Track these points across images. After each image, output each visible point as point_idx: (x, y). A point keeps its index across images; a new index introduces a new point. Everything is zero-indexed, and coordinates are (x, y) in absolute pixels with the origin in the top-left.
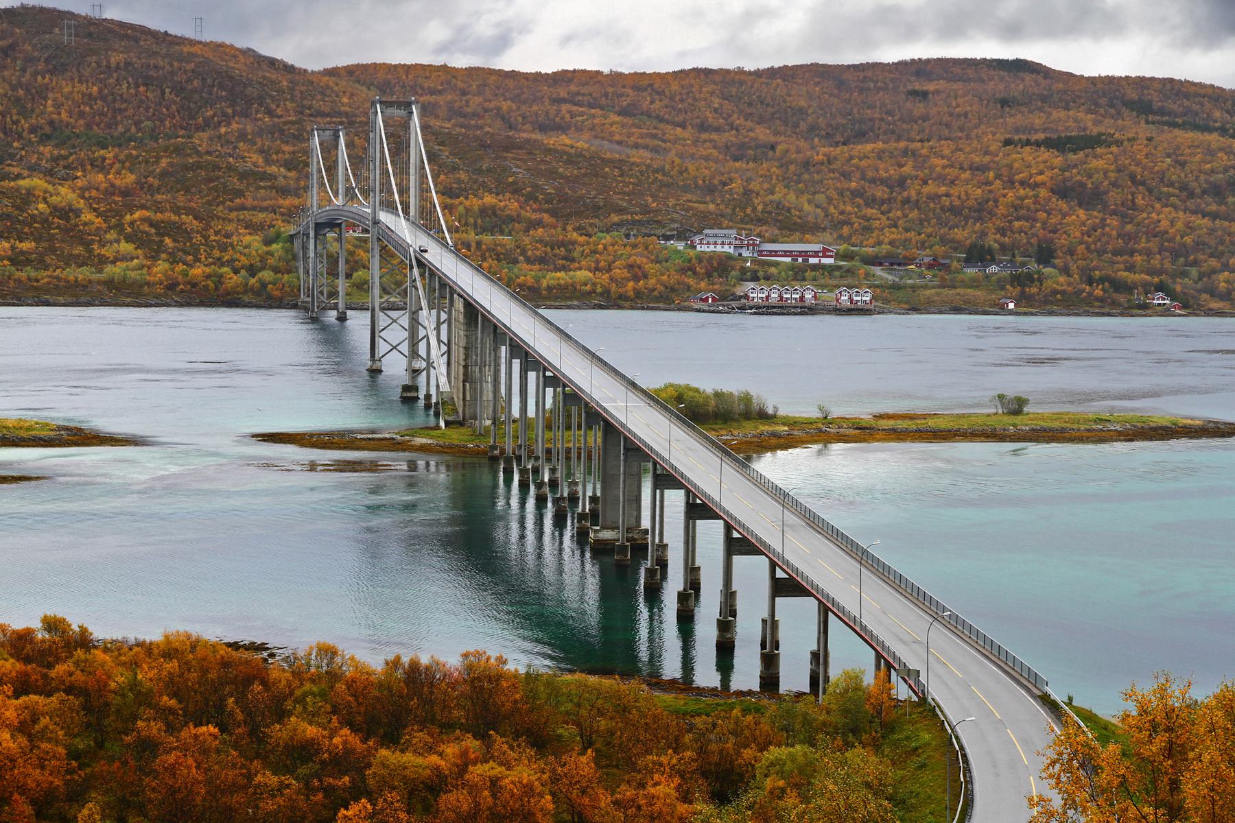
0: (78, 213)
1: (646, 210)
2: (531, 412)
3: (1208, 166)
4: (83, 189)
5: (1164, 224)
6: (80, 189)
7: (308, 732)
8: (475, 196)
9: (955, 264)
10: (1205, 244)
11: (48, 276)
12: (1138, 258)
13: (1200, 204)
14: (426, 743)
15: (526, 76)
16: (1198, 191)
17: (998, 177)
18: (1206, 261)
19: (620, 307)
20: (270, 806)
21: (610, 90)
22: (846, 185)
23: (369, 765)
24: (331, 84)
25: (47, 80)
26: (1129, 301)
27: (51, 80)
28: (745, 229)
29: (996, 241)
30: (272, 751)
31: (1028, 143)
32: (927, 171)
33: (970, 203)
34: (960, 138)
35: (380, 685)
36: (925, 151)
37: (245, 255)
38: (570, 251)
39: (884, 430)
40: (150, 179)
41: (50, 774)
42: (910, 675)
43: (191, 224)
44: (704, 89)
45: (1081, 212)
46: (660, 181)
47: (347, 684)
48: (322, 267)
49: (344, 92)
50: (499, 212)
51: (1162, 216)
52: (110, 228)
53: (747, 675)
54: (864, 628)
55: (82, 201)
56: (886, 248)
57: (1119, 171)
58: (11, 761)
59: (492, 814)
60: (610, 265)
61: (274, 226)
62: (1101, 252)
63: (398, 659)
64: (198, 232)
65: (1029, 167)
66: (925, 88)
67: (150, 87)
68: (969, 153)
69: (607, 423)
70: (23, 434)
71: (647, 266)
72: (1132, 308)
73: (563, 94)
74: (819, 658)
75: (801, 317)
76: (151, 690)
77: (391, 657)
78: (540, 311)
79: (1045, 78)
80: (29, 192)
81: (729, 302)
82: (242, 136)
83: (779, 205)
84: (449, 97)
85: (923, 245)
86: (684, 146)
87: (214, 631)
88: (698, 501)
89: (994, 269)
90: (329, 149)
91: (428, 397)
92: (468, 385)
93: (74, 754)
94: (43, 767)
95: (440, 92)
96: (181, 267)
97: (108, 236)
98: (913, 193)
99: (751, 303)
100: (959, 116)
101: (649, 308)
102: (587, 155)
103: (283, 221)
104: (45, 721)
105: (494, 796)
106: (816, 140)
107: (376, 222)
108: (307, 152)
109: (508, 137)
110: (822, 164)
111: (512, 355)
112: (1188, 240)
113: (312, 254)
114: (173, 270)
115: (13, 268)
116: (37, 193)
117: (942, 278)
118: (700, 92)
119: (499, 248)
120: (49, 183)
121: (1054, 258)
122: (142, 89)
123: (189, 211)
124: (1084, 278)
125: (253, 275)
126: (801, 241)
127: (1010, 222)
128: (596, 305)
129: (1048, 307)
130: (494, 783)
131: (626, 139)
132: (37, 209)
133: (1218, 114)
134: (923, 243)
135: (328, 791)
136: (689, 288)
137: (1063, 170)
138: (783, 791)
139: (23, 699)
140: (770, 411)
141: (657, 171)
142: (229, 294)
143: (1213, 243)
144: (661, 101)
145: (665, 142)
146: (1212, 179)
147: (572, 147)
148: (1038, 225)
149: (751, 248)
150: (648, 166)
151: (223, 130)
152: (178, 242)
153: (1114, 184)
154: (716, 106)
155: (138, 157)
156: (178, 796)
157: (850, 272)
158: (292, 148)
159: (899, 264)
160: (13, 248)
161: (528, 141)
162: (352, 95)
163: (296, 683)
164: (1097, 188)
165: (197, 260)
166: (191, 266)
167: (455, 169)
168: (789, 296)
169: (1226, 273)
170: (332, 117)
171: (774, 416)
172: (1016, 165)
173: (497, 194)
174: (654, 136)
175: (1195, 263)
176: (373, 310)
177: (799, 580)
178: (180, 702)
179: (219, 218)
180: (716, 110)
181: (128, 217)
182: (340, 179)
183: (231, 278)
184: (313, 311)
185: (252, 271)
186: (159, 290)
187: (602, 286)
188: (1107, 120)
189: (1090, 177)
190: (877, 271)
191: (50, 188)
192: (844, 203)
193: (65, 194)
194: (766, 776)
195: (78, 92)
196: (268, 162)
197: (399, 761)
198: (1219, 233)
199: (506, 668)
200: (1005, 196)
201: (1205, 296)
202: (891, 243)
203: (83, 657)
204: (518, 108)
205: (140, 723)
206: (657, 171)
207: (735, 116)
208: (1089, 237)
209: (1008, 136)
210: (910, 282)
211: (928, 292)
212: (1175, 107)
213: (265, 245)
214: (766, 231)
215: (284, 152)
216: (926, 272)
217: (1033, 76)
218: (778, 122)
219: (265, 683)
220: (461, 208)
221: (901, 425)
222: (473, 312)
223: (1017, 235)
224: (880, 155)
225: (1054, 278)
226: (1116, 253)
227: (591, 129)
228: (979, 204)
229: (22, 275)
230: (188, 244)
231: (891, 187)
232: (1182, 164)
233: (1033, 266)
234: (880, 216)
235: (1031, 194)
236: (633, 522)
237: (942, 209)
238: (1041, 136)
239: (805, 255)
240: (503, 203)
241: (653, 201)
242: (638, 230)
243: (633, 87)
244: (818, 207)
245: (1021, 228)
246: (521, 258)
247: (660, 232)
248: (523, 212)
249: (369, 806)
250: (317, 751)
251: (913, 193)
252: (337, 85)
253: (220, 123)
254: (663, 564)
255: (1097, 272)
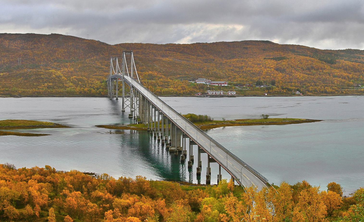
0: (61, 77)
1: (185, 74)
2: (157, 120)
3: (307, 64)
4: (63, 72)
5: (298, 76)
6: (62, 72)
7: (100, 194)
8: (147, 72)
9: (254, 85)
10: (307, 80)
11: (55, 91)
12: (293, 84)
13: (305, 72)
14: (127, 197)
15: (159, 45)
16: (305, 69)
17: (263, 66)
18: (307, 84)
19: (180, 96)
20: (90, 210)
21: (177, 48)
22: (230, 68)
23: (113, 202)
24: (116, 48)
25: (56, 49)
26: (291, 93)
27: (57, 49)
28: (207, 78)
29: (263, 80)
30: (92, 198)
31: (269, 59)
32: (247, 65)
33: (257, 72)
34: (255, 58)
35: (117, 184)
36: (247, 61)
37: (96, 86)
38: (168, 83)
39: (237, 123)
40: (77, 69)
41: (44, 201)
42: (238, 180)
43: (85, 79)
44: (199, 47)
45: (281, 74)
46: (188, 68)
47: (110, 183)
48: (113, 88)
49: (119, 49)
50: (152, 75)
51: (298, 74)
52: (68, 80)
53: (203, 181)
54: (228, 169)
55: (62, 74)
56: (239, 82)
57: (288, 65)
58: (36, 197)
59: (140, 214)
60: (177, 87)
61: (103, 79)
62: (285, 83)
63: (122, 177)
64: (86, 81)
65: (269, 64)
66: (247, 47)
67: (77, 50)
68: (257, 61)
69: (173, 123)
70: (47, 125)
71: (186, 87)
72: (292, 95)
73: (167, 49)
74: (220, 176)
75: (220, 98)
76: (67, 183)
77: (120, 177)
78: (159, 97)
79: (273, 45)
80: (52, 73)
81: (204, 95)
82: (96, 60)
83: (215, 73)
84: (142, 50)
85: (247, 81)
86: (194, 60)
87: (82, 170)
88: (201, 148)
89: (262, 86)
90: (114, 62)
91: (135, 117)
92: (143, 114)
93: (50, 196)
94: (43, 199)
95: (140, 49)
96: (82, 88)
97: (67, 82)
98: (244, 70)
99: (209, 95)
100: (254, 53)
101: (186, 96)
102: (172, 62)
103: (105, 78)
104: (44, 189)
105: (141, 210)
106: (223, 58)
107: (124, 78)
108: (110, 63)
109: (154, 58)
110: (224, 64)
111: (152, 108)
112: (303, 79)
113: (110, 85)
114: (81, 89)
115: (47, 89)
116: (53, 73)
117: (251, 88)
118: (198, 48)
119: (152, 83)
120: (56, 71)
121: (275, 84)
122: (76, 50)
123: (84, 76)
124: (282, 88)
125: (98, 90)
126: (220, 81)
127: (266, 76)
128: (174, 96)
129: (274, 95)
130: (141, 208)
131: (181, 58)
132: (53, 76)
133: (309, 53)
134: (247, 81)
135: (104, 207)
136: (195, 91)
137: (276, 65)
138: (207, 208)
139: (40, 184)
140: (212, 119)
141: (188, 66)
142: (93, 94)
143: (308, 80)
144: (189, 50)
145: (190, 59)
146: (308, 67)
147: (169, 60)
148: (272, 77)
149: (209, 82)
150: (186, 64)
151: (92, 58)
152: (82, 83)
153: (287, 68)
154: (201, 51)
155: (74, 65)
156: (71, 207)
157: (231, 87)
158: (107, 62)
159: (242, 86)
160: (48, 85)
161: (159, 59)
162: (121, 50)
163: (98, 183)
164: (284, 68)
165: (86, 87)
166: (85, 88)
167: (143, 66)
168: (217, 93)
169: (311, 87)
170: (116, 55)
171: (213, 120)
172: (267, 64)
173: (152, 71)
174: (187, 58)
175: (305, 85)
176: (123, 97)
177: (214, 158)
178: (73, 186)
179: (91, 77)
180: (201, 52)
181: (72, 78)
182: (117, 68)
183: (93, 91)
184: (111, 98)
185: (98, 89)
186: (78, 93)
187: (176, 91)
188: (286, 54)
189: (282, 66)
190: (237, 87)
191: (56, 72)
192: (230, 72)
193: (59, 73)
194: (204, 204)
195: (62, 51)
196: (102, 65)
197: (120, 201)
198: (309, 78)
199: (146, 180)
200: (264, 70)
201: (307, 92)
202: (240, 81)
203: (53, 175)
204: (157, 52)
205: (64, 190)
206: (188, 66)
207: (205, 53)
208: (283, 79)
209: (265, 57)
210: (244, 89)
211: (248, 92)
212: (300, 51)
213: (101, 83)
214: (212, 79)
215: (105, 63)
216: (248, 87)
217: (270, 44)
218: (215, 54)
219: (91, 182)
220: (144, 74)
221: (241, 122)
222: (144, 98)
223: (267, 79)
224: (237, 61)
225: (276, 89)
226: (288, 83)
227: (174, 56)
228: (259, 72)
229: (49, 90)
230: (84, 83)
231: (240, 69)
232: (302, 63)
233: (271, 86)
234: (237, 75)
235: (270, 70)
236: (179, 146)
237: (251, 73)
238: (272, 57)
239: (221, 84)
240: (153, 73)
241: (187, 72)
242: (184, 79)
243: (182, 47)
244: (224, 73)
245: (268, 77)
246: (157, 85)
247: (189, 79)
248: (158, 75)
249: (112, 211)
250: (102, 198)
251: (244, 70)
252: (117, 48)
253: (92, 57)
254: (185, 155)
255: (284, 87)
